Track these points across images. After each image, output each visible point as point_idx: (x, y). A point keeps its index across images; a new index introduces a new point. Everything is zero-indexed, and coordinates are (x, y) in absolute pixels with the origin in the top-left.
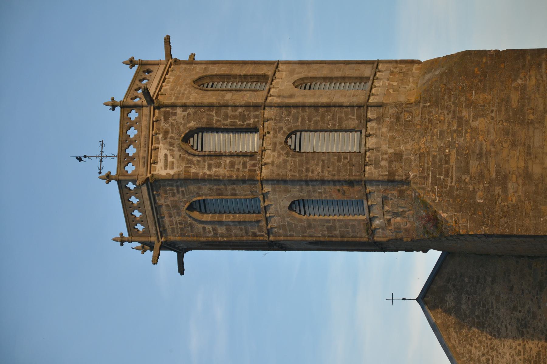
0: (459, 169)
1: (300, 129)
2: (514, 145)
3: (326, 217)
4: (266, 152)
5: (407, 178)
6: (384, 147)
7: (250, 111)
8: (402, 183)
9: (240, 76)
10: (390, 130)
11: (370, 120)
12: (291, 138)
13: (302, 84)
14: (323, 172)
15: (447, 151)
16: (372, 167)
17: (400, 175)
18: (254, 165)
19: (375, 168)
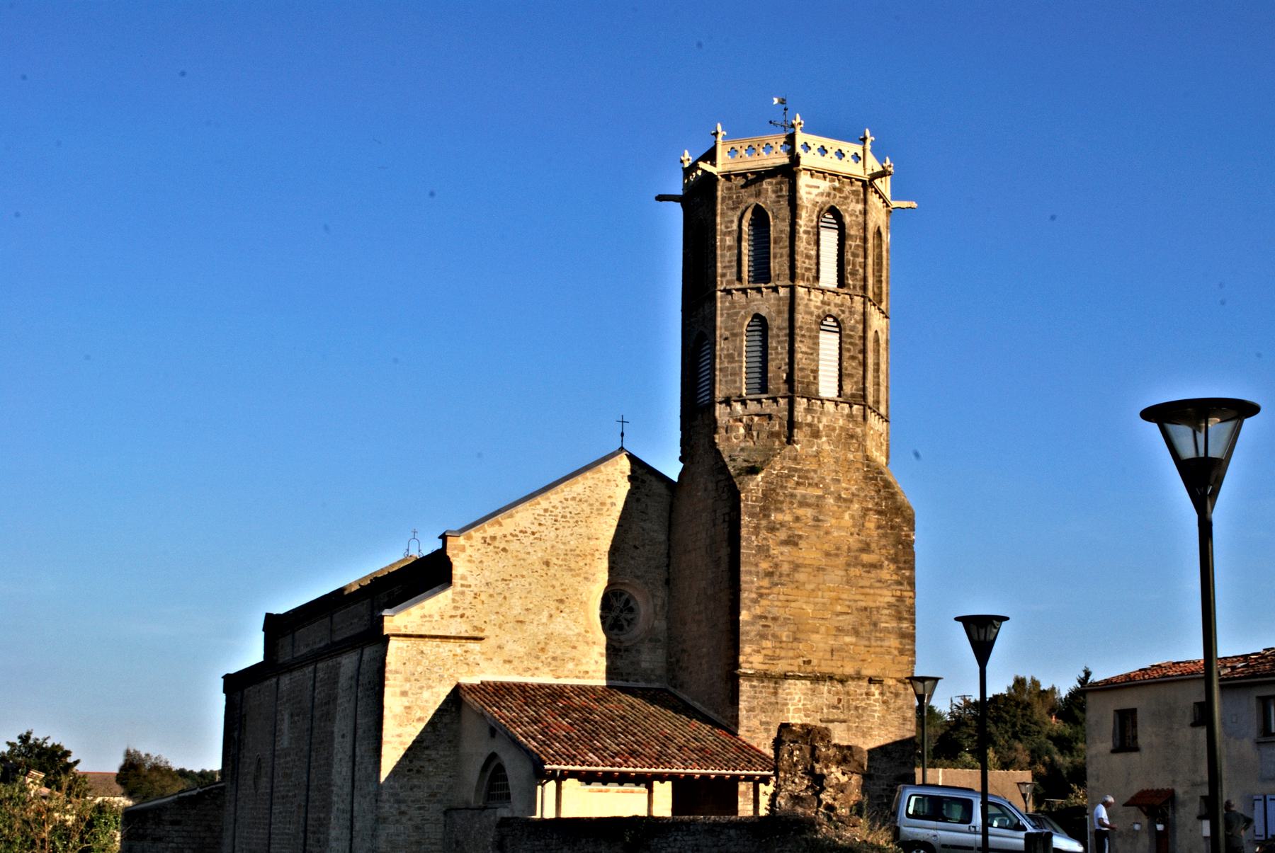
0: (804, 496)
2: (828, 554)
3: (744, 354)
5: (794, 442)
6: (824, 420)
11: (851, 407)
14: (802, 352)
17: (798, 435)
18: (808, 280)
19: (805, 409)
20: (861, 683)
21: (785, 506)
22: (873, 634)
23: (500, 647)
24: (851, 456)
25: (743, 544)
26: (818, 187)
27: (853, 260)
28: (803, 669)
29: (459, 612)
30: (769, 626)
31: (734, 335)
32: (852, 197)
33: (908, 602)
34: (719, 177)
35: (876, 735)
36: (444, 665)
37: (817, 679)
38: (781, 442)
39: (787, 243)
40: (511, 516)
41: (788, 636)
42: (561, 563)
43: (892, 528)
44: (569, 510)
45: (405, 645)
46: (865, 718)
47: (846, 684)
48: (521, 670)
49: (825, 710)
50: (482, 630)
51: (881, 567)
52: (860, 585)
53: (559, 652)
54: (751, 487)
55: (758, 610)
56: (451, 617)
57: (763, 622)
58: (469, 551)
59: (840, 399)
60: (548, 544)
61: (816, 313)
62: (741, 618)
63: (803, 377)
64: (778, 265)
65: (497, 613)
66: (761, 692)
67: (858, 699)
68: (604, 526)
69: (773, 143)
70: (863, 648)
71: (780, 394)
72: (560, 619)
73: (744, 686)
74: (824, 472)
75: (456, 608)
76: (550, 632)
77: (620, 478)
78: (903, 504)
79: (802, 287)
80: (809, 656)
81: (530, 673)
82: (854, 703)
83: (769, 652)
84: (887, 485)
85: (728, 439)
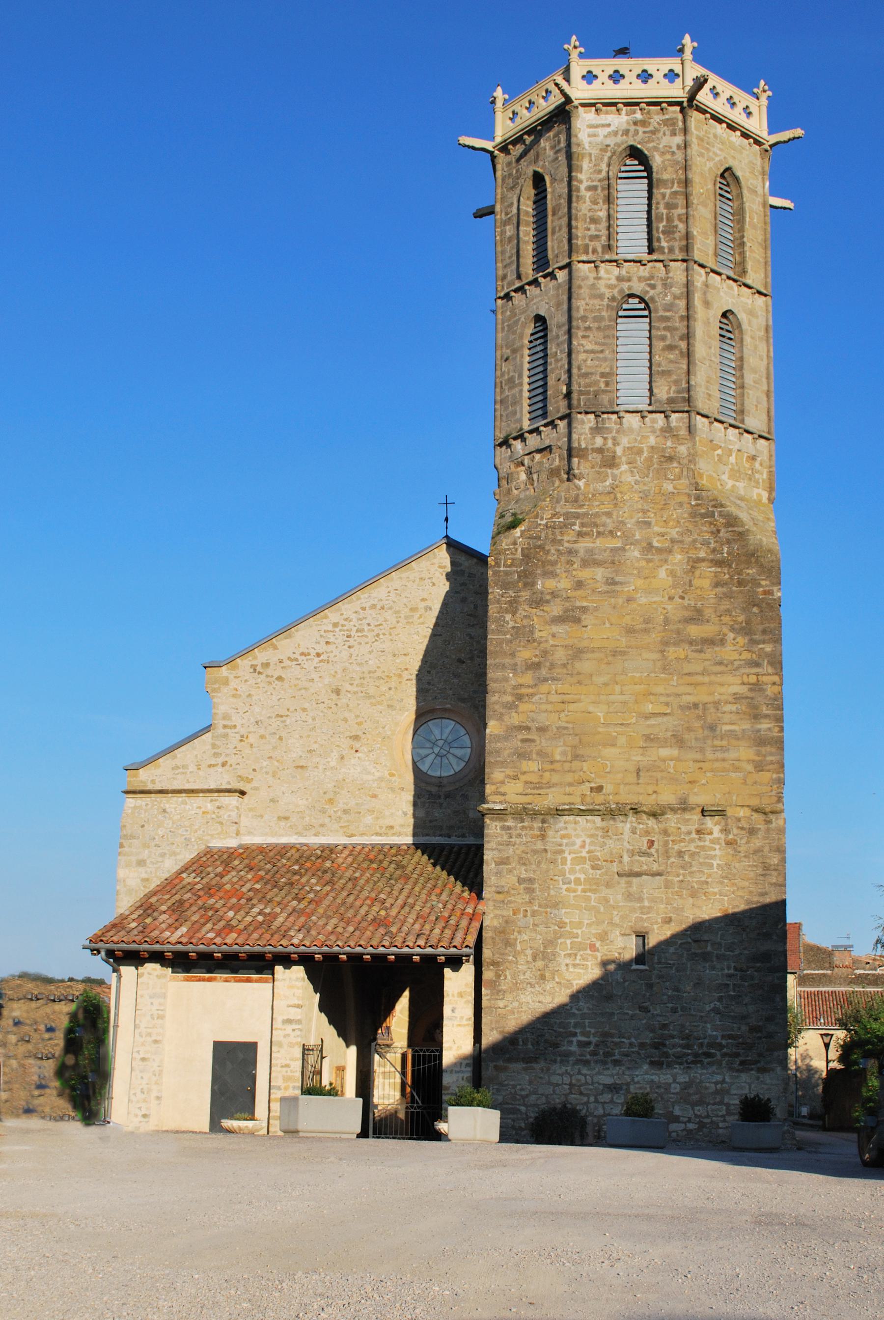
0: (590, 551)
1: (652, 315)
2: (630, 631)
4: (615, 268)
6: (625, 441)
7: (681, 240)
8: (569, 471)
9: (743, 237)
10: (652, 447)
12: (640, 303)
13: (732, 327)
15: (619, 534)
16: (593, 424)
18: (594, 251)
19: (591, 428)
20: (687, 816)
21: (559, 569)
22: (709, 742)
23: (273, 800)
24: (669, 487)
25: (492, 626)
26: (609, 125)
27: (667, 214)
28: (588, 799)
29: (220, 760)
30: (533, 741)
31: (514, 351)
33: (770, 691)
35: (715, 894)
37: (611, 813)
39: (566, 210)
40: (290, 636)
41: (564, 753)
42: (355, 689)
43: (740, 583)
44: (367, 622)
45: (144, 803)
46: (694, 869)
47: (662, 818)
49: (626, 859)
50: (249, 781)
51: (722, 642)
52: (686, 671)
54: (504, 546)
55: (515, 719)
56: (210, 766)
57: (524, 735)
58: (233, 684)
62: (488, 731)
63: (589, 385)
65: (270, 758)
66: (520, 835)
67: (683, 840)
72: (353, 761)
75: (216, 755)
76: (341, 777)
79: (584, 262)
80: (598, 780)
81: (313, 831)
82: (676, 847)
83: (534, 778)
84: (732, 521)
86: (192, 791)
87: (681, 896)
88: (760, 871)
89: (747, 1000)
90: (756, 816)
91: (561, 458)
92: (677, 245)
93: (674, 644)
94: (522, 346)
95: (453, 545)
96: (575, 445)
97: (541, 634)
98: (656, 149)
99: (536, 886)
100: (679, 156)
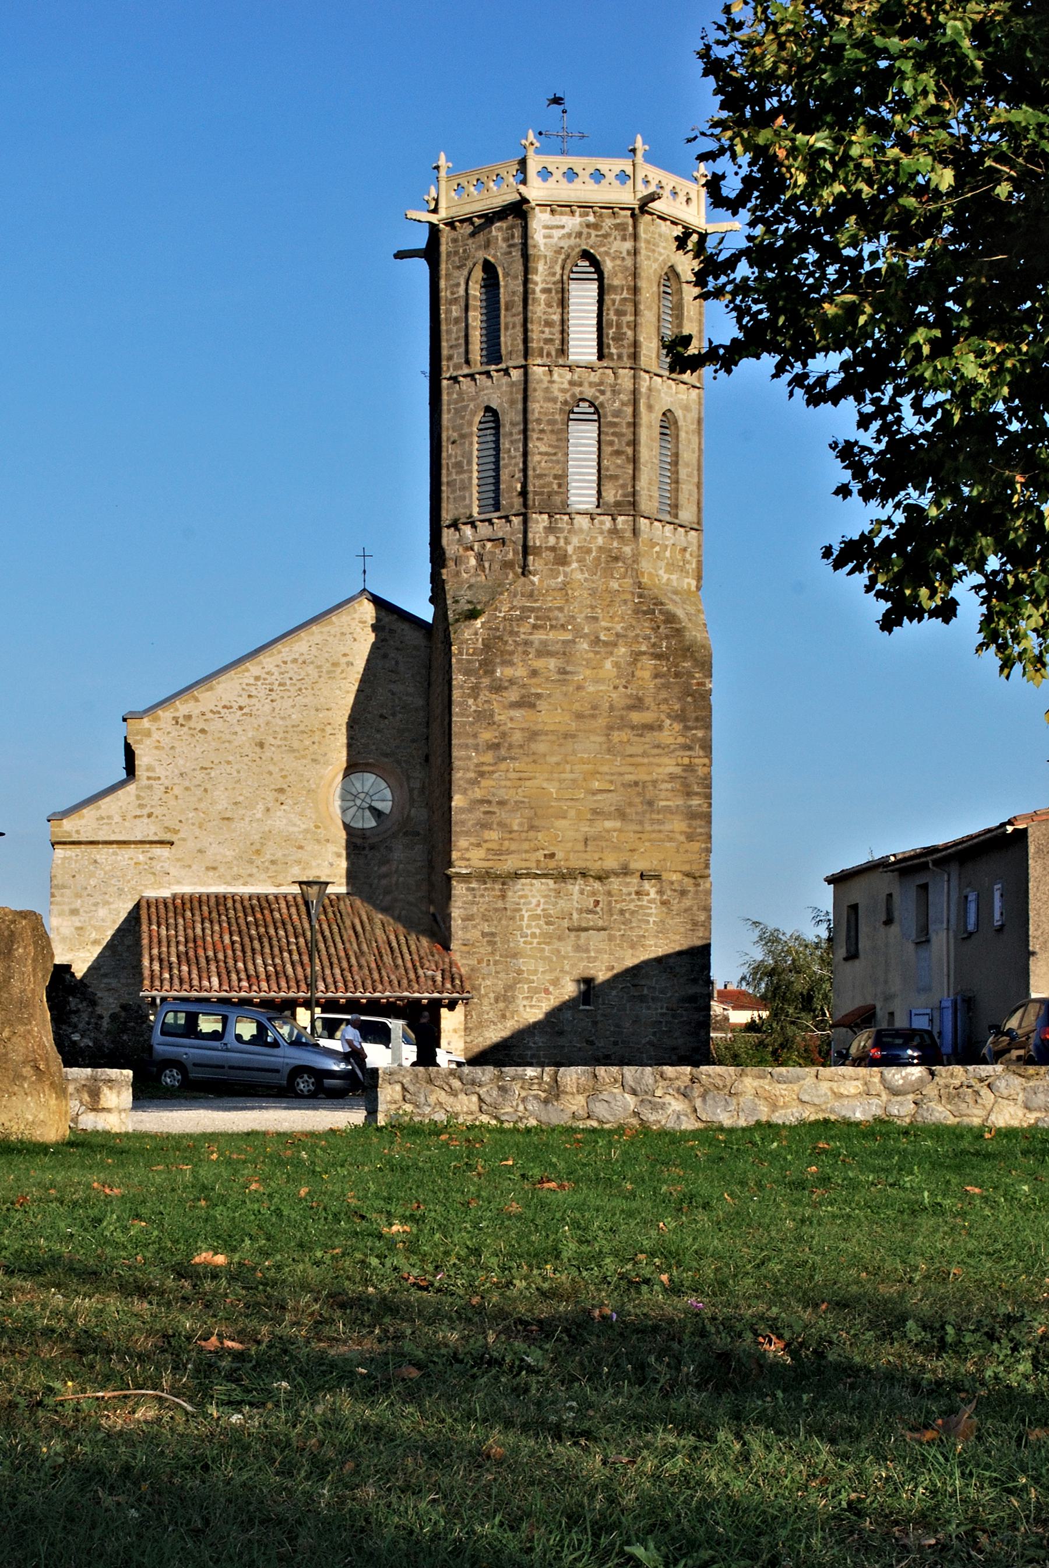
0: (544, 643)
2: (579, 716)
6: (575, 541)
8: (525, 566)
11: (614, 520)
16: (546, 524)
18: (549, 355)
22: (648, 816)
23: (200, 851)
24: (615, 585)
25: (456, 709)
26: (563, 227)
28: (542, 865)
29: (146, 811)
30: (494, 813)
31: (463, 436)
32: (615, 233)
33: (701, 771)
34: (442, 226)
36: (124, 876)
37: (562, 877)
38: (515, 574)
39: (521, 309)
40: (211, 689)
41: (521, 824)
43: (677, 675)
47: (606, 881)
48: (229, 878)
49: (575, 916)
50: (176, 832)
51: (660, 728)
53: (279, 854)
54: (466, 636)
55: (478, 794)
57: (486, 808)
58: (156, 736)
59: (599, 511)
60: (261, 721)
61: (561, 399)
64: (511, 339)
66: (483, 896)
67: (624, 900)
68: (338, 692)
69: (504, 174)
70: (632, 835)
71: (514, 511)
72: (279, 814)
73: (459, 889)
74: (574, 608)
76: (267, 829)
77: (358, 630)
78: (693, 643)
81: (241, 881)
83: (494, 846)
84: (670, 618)
85: (458, 574)
86: (124, 842)
87: (622, 948)
88: (689, 927)
89: (677, 1034)
90: (686, 880)
91: (515, 552)
92: (625, 352)
93: (618, 729)
94: (471, 434)
95: (378, 602)
96: (531, 543)
97: (502, 717)
98: (607, 253)
99: (497, 939)
100: (629, 262)
